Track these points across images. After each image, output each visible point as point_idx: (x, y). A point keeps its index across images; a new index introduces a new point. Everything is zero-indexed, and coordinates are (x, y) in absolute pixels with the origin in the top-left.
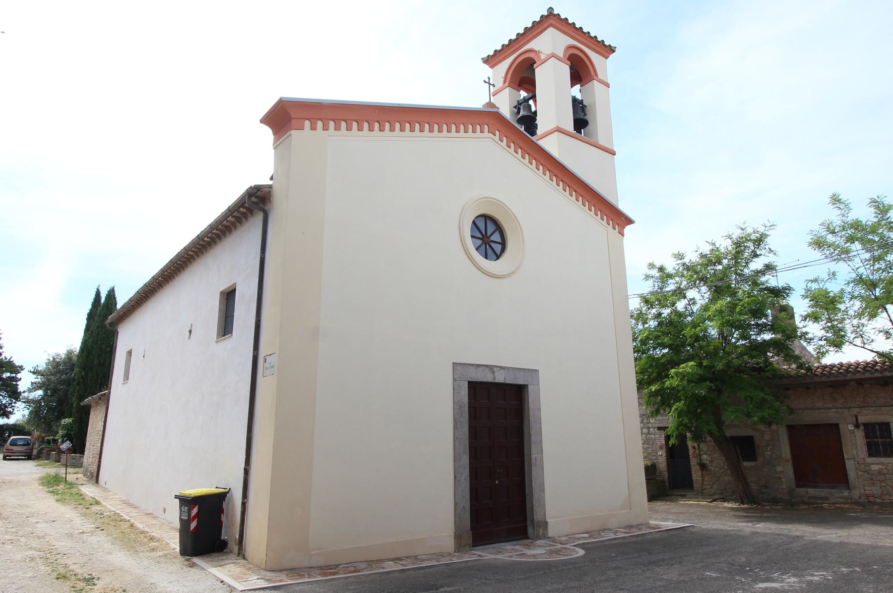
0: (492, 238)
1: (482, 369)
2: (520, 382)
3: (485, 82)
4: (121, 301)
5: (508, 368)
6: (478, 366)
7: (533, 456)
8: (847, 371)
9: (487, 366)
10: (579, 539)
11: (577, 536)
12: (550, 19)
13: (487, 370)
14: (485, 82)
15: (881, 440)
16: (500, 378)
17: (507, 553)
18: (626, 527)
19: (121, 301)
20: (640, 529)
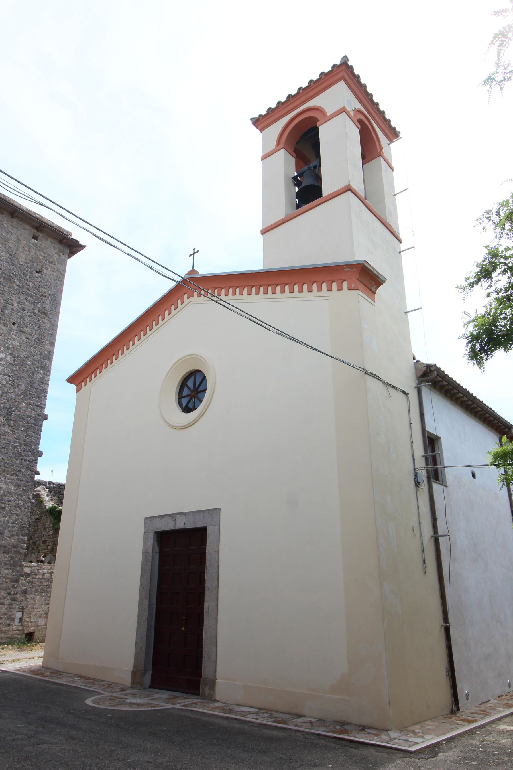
0: (189, 393)
1: (166, 518)
2: (199, 525)
3: (194, 249)
4: (436, 486)
5: (188, 513)
6: (163, 516)
7: (206, 604)
8: (58, 304)
9: (169, 515)
10: (237, 713)
11: (237, 708)
12: (343, 72)
13: (170, 519)
14: (194, 249)
15: (2, 638)
16: (180, 524)
17: (183, 703)
18: (337, 722)
19: (436, 486)
20: (345, 732)
